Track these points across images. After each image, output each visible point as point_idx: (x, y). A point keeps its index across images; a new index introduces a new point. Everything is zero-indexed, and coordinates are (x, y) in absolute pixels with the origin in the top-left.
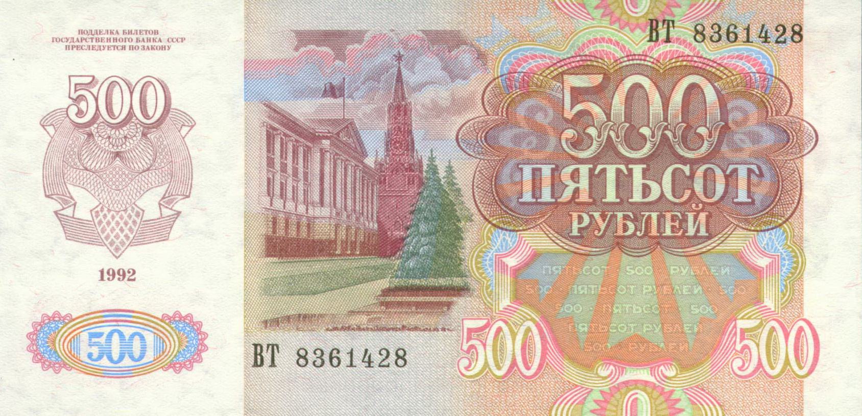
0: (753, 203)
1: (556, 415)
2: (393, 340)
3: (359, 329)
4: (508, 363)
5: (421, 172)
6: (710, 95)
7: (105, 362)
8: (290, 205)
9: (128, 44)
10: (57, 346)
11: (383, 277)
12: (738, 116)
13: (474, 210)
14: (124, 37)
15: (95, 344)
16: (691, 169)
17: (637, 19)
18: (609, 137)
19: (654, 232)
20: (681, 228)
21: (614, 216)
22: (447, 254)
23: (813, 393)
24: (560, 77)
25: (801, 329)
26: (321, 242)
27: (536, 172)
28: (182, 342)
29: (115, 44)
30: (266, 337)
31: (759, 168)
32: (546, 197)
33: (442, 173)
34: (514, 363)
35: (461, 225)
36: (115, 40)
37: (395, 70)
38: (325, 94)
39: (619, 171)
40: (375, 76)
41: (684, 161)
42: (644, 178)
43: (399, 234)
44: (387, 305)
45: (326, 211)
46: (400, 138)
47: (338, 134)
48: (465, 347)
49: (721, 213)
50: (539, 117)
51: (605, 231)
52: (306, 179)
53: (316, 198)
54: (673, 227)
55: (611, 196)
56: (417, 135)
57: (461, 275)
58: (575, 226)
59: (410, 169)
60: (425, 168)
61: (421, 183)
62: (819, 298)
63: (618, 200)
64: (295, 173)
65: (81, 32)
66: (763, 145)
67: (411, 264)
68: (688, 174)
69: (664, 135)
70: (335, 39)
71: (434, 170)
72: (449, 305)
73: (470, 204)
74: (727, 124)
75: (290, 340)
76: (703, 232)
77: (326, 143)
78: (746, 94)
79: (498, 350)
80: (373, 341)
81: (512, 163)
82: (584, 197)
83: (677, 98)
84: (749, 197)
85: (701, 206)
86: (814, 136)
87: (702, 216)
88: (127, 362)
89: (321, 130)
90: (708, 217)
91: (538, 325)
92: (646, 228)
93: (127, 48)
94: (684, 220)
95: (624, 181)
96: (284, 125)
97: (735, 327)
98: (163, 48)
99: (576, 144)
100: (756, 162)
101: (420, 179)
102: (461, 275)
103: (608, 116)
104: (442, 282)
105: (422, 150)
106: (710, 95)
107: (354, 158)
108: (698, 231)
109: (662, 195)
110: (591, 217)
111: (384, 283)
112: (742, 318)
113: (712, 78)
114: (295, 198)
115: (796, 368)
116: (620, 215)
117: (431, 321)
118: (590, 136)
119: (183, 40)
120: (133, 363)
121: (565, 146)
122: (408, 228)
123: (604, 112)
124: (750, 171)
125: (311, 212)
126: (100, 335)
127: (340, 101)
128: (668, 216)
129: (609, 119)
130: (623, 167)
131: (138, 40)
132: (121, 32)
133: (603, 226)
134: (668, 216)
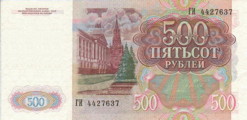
0: (217, 58)
1: (207, 1)
2: (115, 98)
3: (105, 94)
4: (147, 106)
5: (123, 49)
6: (206, 28)
7: (32, 106)
8: (86, 59)
9: (40, 12)
10: (19, 101)
11: (112, 79)
12: (213, 33)
13: (138, 60)
14: (38, 10)
15: (30, 101)
16: (200, 49)
17: (184, 7)
18: (176, 39)
19: (189, 67)
20: (197, 65)
21: (178, 62)
22: (131, 74)
23: (233, 116)
24: (162, 22)
25: (230, 97)
26: (95, 70)
27: (156, 49)
28: (54, 100)
29: (36, 12)
30: (80, 97)
31: (219, 48)
32: (158, 57)
33: (129, 49)
34: (149, 107)
35: (135, 64)
36: (36, 11)
37: (115, 20)
38: (96, 27)
39: (179, 49)
40: (110, 21)
41: (198, 46)
42: (186, 51)
43: (116, 67)
44: (113, 87)
45: (96, 61)
46: (117, 40)
47: (99, 38)
48: (135, 102)
49: (209, 62)
50: (157, 33)
51: (175, 66)
52: (90, 51)
53: (93, 57)
54: (195, 65)
55: (177, 56)
56: (122, 38)
57: (135, 79)
58: (167, 65)
59: (120, 48)
60: (124, 48)
61: (123, 52)
62: (235, 87)
63: (179, 57)
64: (87, 50)
65: (27, 9)
66: (219, 42)
67: (121, 75)
68: (199, 50)
69: (192, 38)
70: (99, 11)
71: (127, 48)
72: (131, 87)
73: (137, 58)
74: (210, 35)
75: (86, 98)
76: (203, 67)
77: (96, 41)
78: (216, 27)
79: (144, 103)
80: (110, 98)
81: (149, 46)
82: (169, 56)
83: (196, 28)
84: (216, 57)
85: (202, 59)
86: (235, 39)
87: (203, 62)
88: (39, 106)
89: (95, 37)
90: (204, 63)
91: (156, 96)
92: (187, 66)
93: (40, 14)
94: (198, 63)
95: (181, 52)
96: (85, 36)
97: (212, 96)
98: (50, 13)
99: (168, 41)
100: (219, 47)
101: (123, 51)
102: (135, 79)
103: (176, 33)
104: (129, 80)
105: (123, 42)
106: (206, 28)
107: (104, 46)
108: (201, 66)
109: (191, 56)
110: (171, 62)
111: (113, 81)
112: (213, 94)
113: (206, 22)
114: (87, 57)
115: (229, 109)
116: (179, 62)
117: (126, 92)
118: (171, 39)
119: (55, 11)
120: (41, 107)
121: (163, 41)
122: (119, 65)
123: (175, 32)
124: (216, 49)
125: (92, 61)
126: (31, 99)
127: (100, 28)
128: (193, 62)
129: (176, 34)
130: (180, 48)
131: (42, 11)
132: (38, 9)
133: (174, 65)
134: (193, 62)
